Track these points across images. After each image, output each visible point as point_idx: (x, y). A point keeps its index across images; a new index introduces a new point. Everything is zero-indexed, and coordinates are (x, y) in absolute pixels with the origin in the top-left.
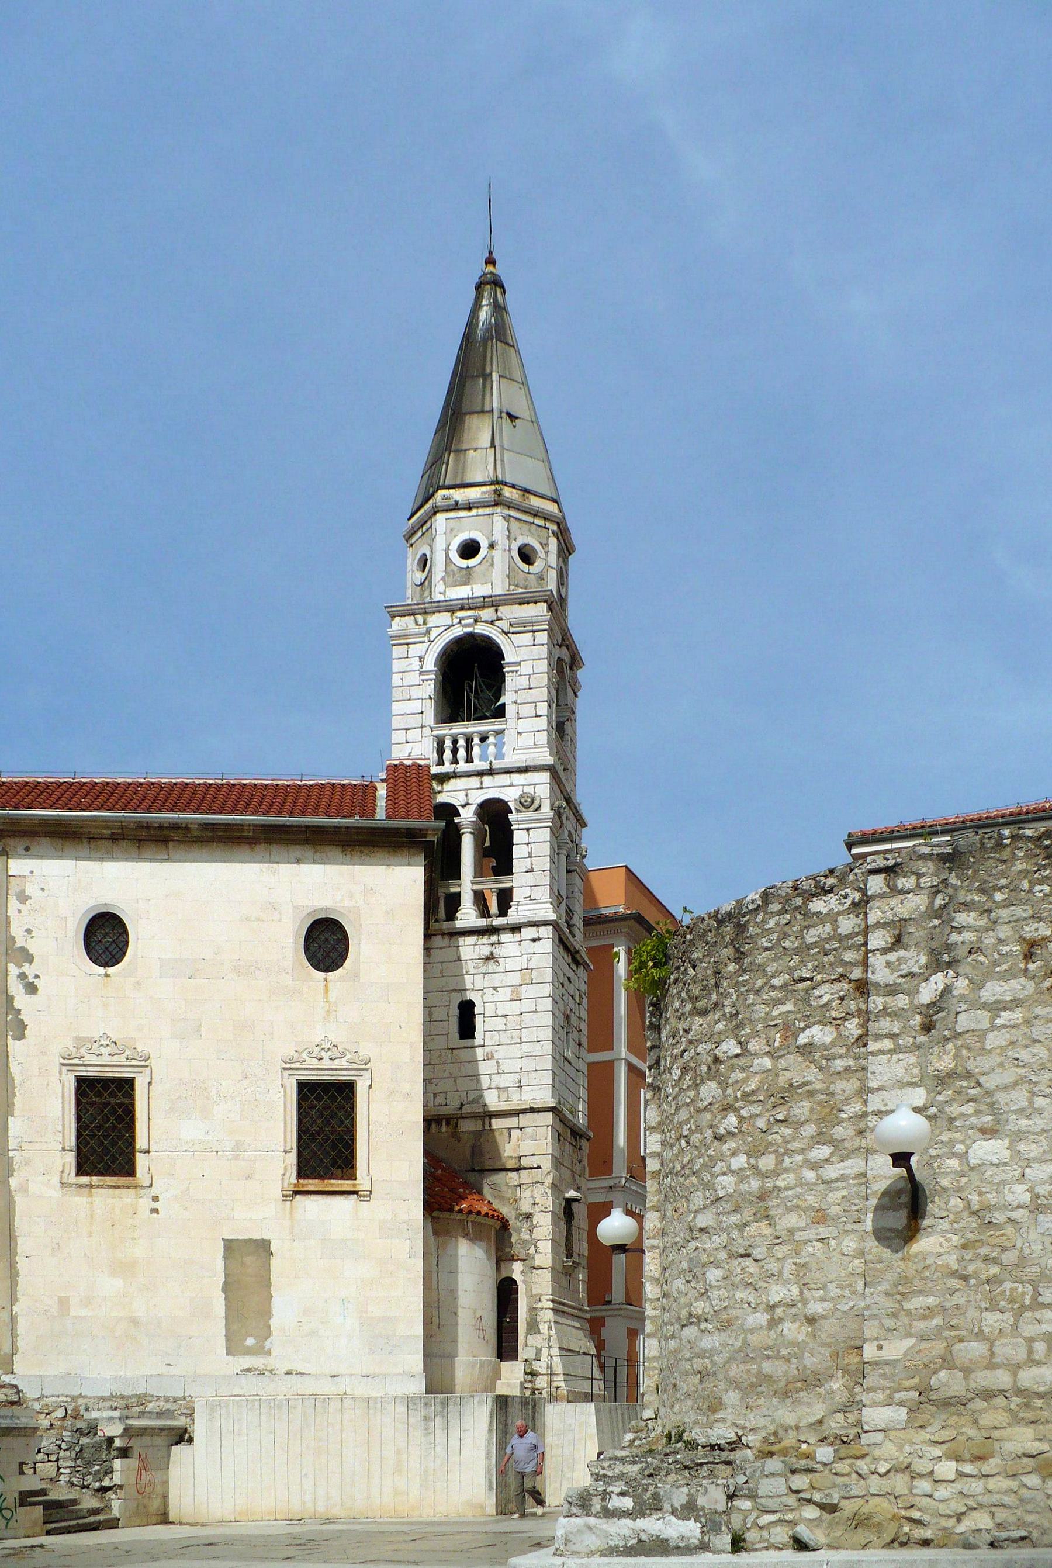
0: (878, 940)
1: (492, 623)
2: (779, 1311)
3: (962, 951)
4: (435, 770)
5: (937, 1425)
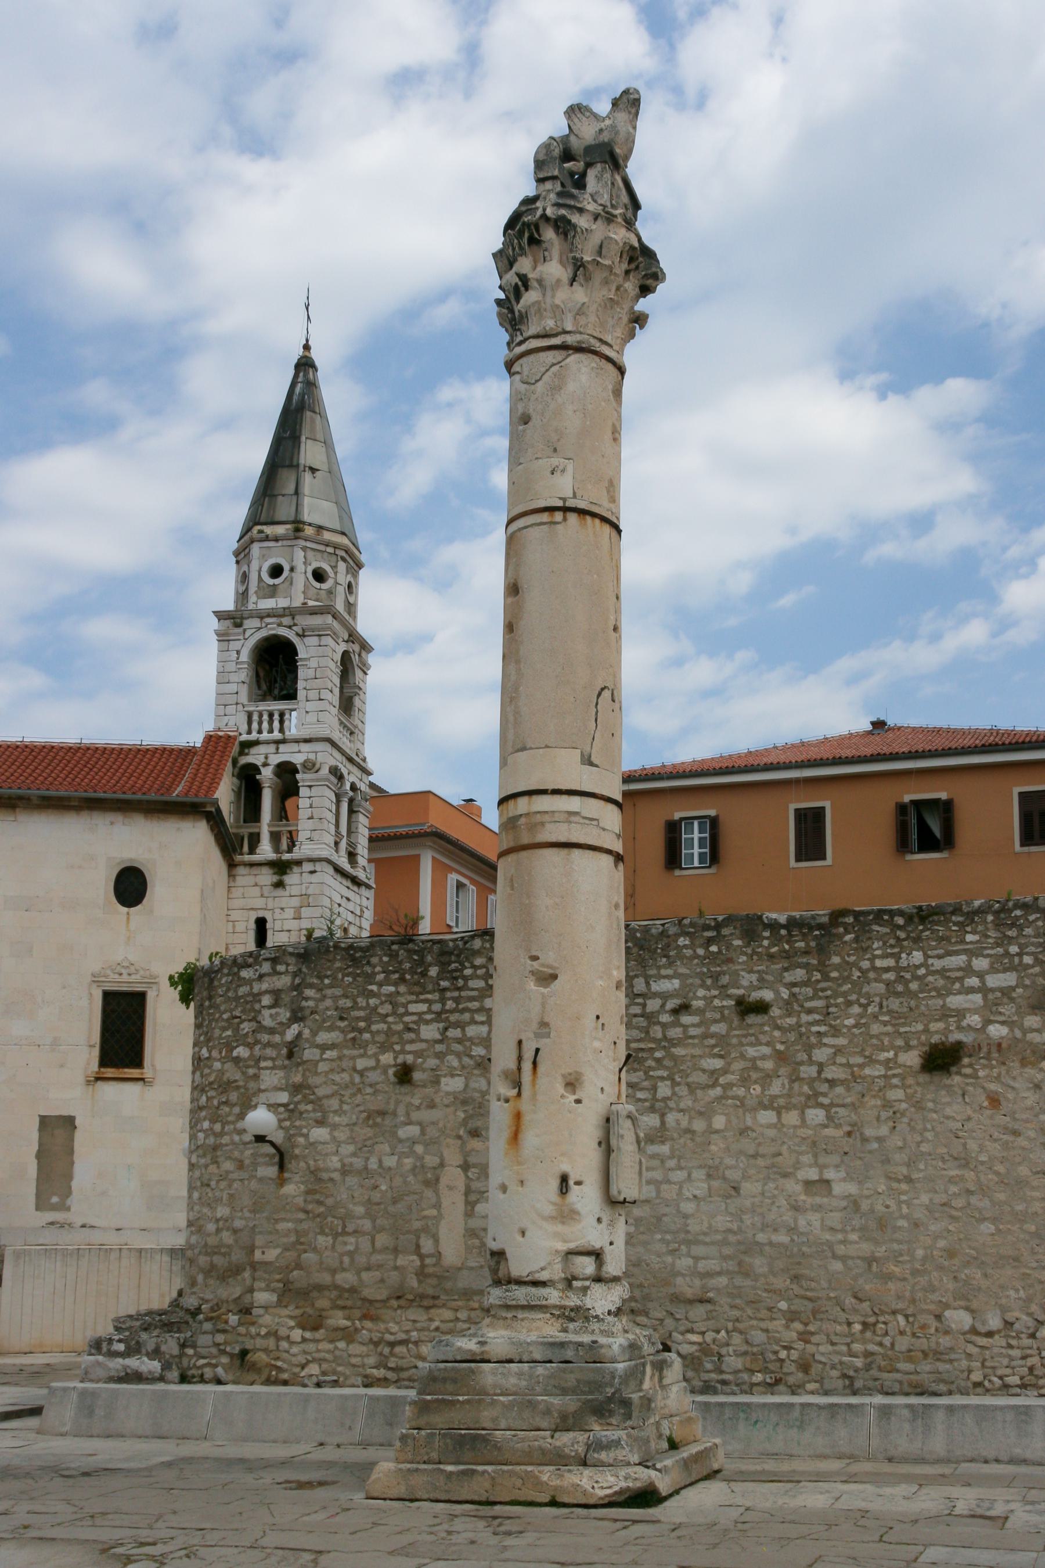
0: (266, 1000)
1: (290, 627)
2: (221, 1223)
3: (307, 1012)
4: (244, 737)
5: (291, 1308)
